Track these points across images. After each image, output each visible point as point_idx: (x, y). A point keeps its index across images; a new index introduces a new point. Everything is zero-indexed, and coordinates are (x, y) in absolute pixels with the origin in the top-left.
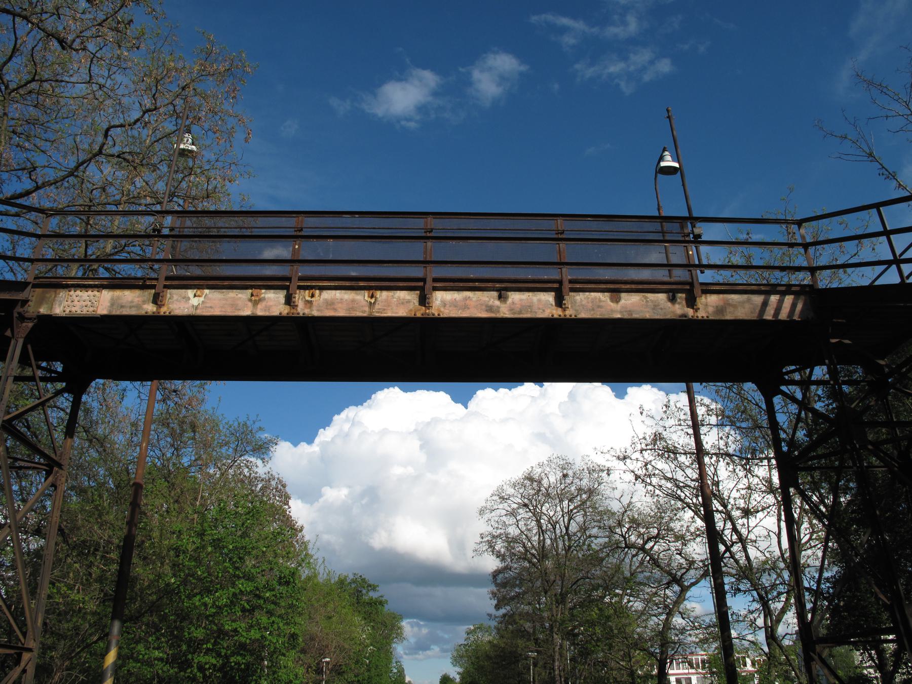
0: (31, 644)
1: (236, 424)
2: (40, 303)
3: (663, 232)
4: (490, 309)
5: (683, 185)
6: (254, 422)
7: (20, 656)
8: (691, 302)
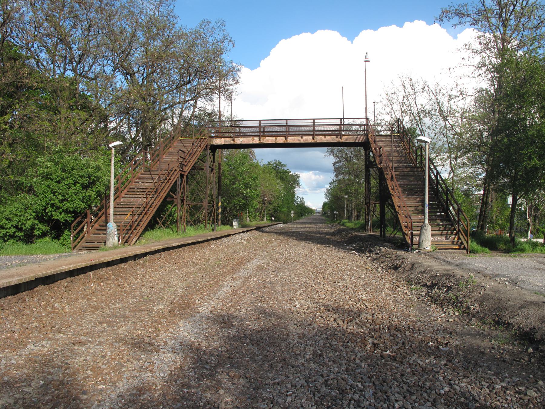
4: (299, 140)
5: (365, 71)
8: (341, 138)
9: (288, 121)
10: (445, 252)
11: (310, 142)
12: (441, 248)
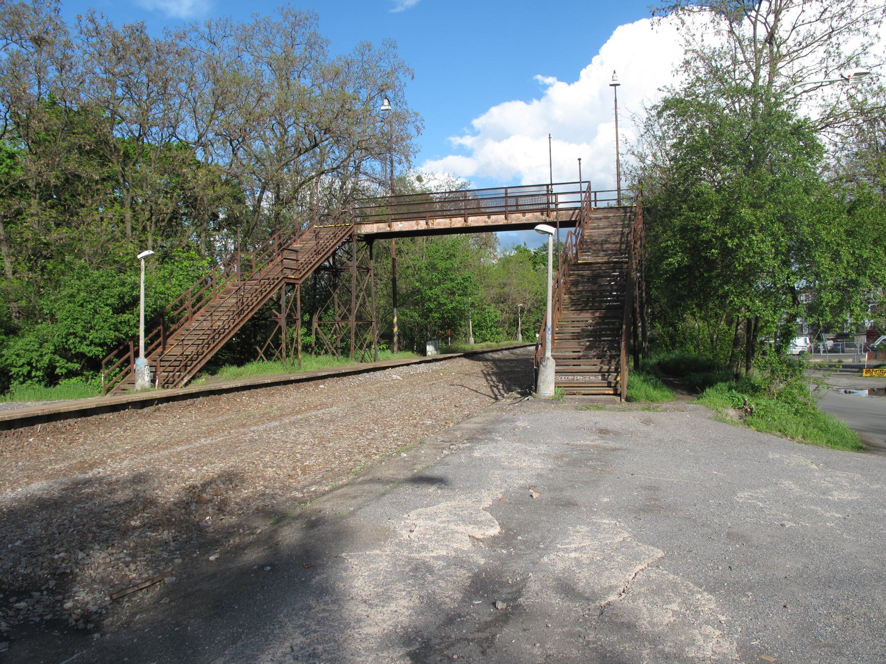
3: (517, 205)
5: (616, 101)
9: (509, 190)
10: (599, 401)
11: (501, 223)
12: (587, 392)
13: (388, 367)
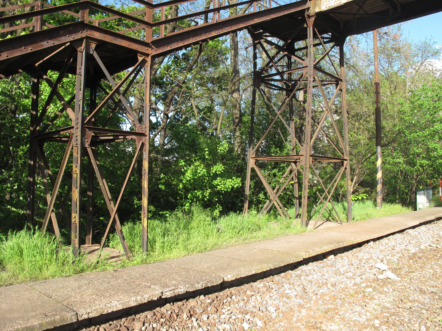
0: (346, 157)
1: (420, 44)
2: (314, 7)
5: (360, 245)
6: (430, 40)
7: (343, 162)
13: (368, 242)
